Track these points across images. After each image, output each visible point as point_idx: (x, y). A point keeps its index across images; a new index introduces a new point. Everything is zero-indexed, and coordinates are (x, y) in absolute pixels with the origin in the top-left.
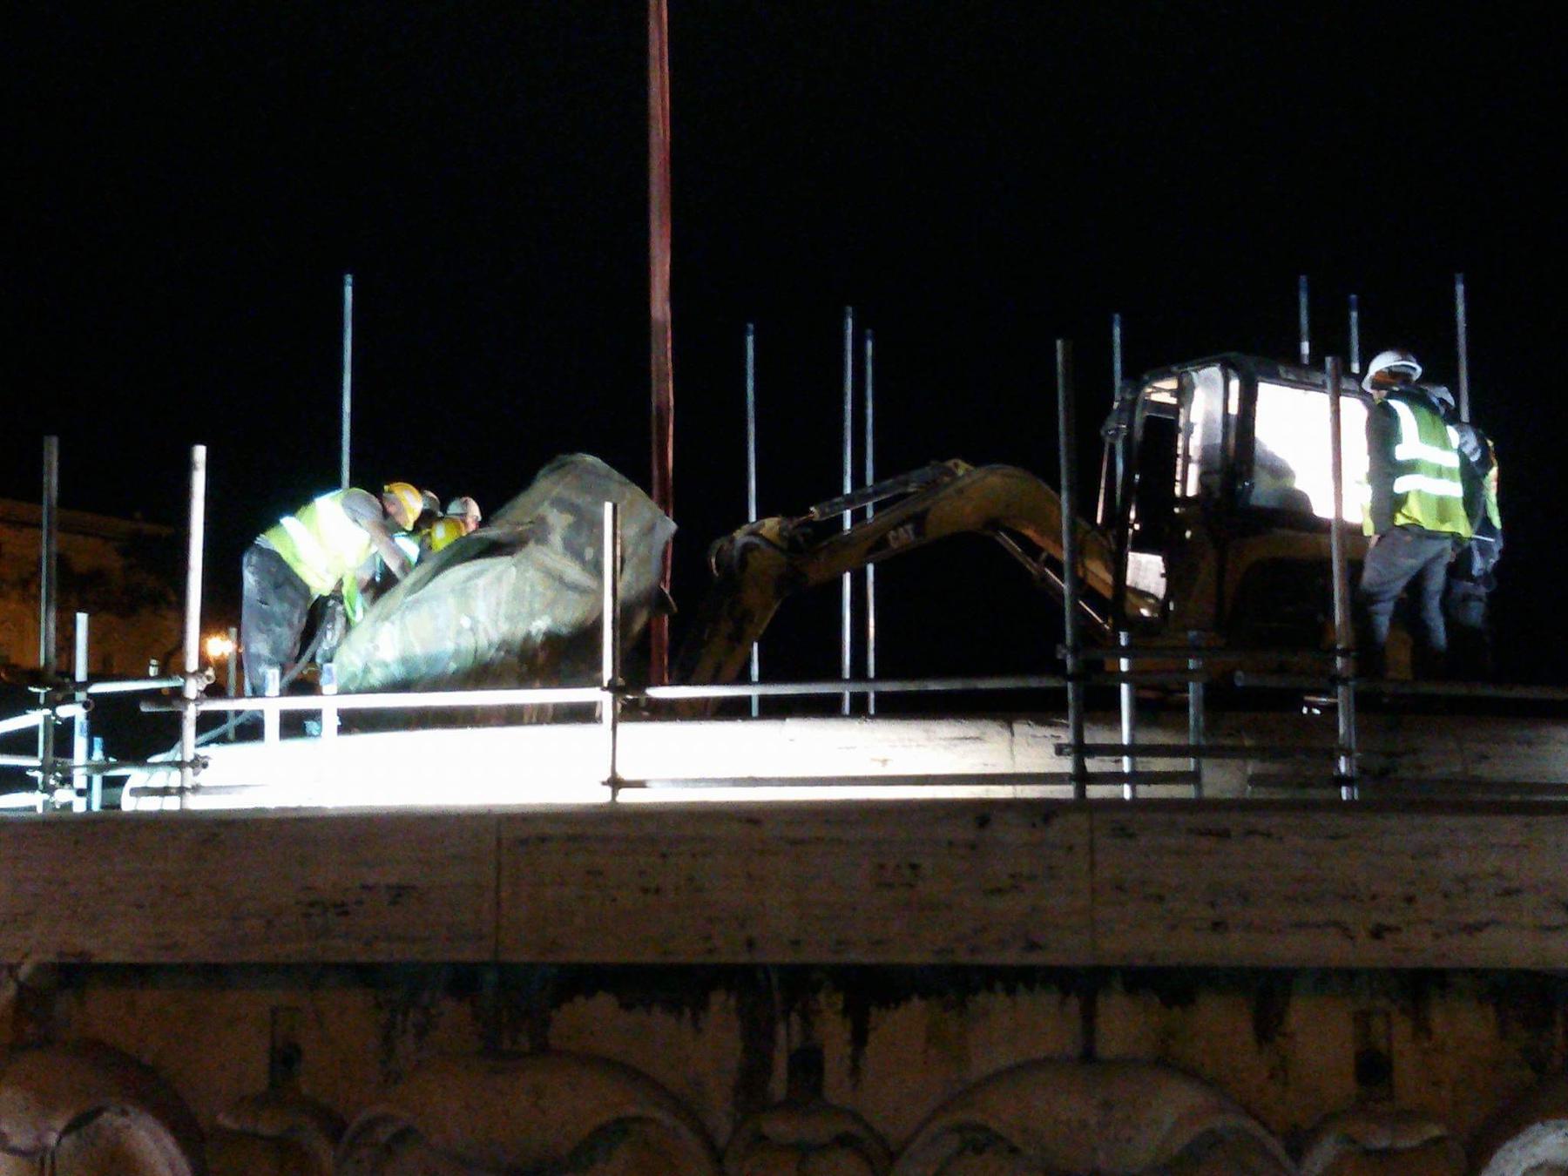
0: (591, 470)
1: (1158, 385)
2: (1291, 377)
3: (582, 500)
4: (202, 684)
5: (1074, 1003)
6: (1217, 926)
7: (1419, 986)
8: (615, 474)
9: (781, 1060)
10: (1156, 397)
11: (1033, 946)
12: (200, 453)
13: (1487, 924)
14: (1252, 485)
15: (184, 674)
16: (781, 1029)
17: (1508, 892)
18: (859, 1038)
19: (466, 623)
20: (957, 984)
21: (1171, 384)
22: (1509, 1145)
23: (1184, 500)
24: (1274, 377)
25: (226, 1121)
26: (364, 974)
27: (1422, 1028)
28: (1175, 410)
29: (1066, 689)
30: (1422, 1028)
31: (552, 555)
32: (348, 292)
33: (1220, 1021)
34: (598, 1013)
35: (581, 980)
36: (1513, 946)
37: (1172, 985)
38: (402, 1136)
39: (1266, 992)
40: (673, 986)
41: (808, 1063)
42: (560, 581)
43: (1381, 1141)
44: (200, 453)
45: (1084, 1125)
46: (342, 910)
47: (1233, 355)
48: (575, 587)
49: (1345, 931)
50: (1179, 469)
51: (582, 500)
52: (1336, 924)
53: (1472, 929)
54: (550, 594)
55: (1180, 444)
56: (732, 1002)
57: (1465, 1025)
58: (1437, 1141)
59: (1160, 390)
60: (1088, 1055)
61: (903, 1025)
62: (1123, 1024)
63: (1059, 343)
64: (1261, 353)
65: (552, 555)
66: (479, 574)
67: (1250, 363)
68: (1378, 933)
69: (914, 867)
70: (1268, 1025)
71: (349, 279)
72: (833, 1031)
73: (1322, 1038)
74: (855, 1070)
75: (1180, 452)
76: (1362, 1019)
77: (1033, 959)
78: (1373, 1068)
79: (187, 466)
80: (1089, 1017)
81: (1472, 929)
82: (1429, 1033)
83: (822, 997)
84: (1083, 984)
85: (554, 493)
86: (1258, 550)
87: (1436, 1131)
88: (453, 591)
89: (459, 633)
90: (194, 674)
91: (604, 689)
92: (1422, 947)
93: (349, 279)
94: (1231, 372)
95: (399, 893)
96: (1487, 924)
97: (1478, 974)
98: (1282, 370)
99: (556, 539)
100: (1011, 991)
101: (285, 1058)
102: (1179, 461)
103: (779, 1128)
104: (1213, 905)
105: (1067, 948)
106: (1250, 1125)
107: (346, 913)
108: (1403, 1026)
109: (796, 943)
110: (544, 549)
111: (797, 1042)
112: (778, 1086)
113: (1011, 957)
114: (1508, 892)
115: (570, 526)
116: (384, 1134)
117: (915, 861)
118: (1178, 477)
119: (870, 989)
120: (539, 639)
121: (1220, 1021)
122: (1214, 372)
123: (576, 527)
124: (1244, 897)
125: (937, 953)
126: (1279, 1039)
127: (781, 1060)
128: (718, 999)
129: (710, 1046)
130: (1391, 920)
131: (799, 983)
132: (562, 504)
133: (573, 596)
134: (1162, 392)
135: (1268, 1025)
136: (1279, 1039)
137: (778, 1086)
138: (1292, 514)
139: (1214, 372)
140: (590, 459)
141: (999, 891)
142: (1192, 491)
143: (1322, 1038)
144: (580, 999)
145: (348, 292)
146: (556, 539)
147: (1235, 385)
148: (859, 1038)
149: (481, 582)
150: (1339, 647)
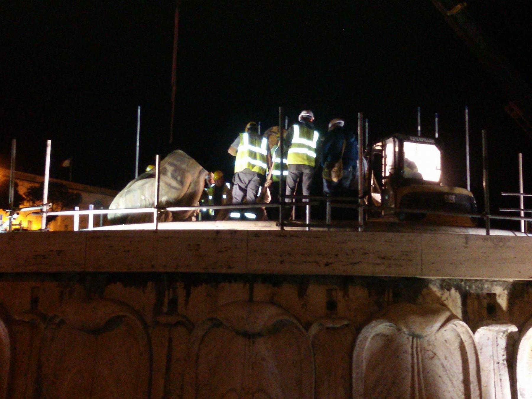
0: (181, 155)
1: (377, 144)
2: (414, 140)
3: (178, 163)
4: (48, 208)
5: (248, 285)
6: (282, 262)
7: (346, 281)
8: (187, 156)
9: (166, 301)
10: (377, 148)
11: (230, 267)
12: (49, 142)
13: (358, 263)
14: (403, 172)
15: (43, 205)
16: (167, 293)
17: (365, 254)
18: (188, 295)
19: (143, 198)
20: (215, 279)
21: (380, 144)
22: (366, 327)
23: (385, 177)
24: (409, 140)
25: (17, 318)
26: (56, 276)
27: (346, 294)
28: (381, 151)
29: (278, 208)
30: (346, 294)
31: (168, 179)
32: (139, 111)
33: (288, 292)
34: (117, 289)
35: (114, 278)
36: (366, 269)
37: (274, 280)
38: (62, 322)
39: (302, 283)
40: (135, 279)
41: (173, 303)
42: (170, 186)
43: (330, 325)
44: (49, 142)
45: (243, 318)
46: (44, 257)
47: (397, 134)
48: (175, 188)
49: (317, 263)
50: (383, 168)
51: (178, 163)
52: (315, 262)
53: (354, 264)
54: (167, 189)
55: (383, 161)
56: (154, 285)
57: (358, 294)
58: (347, 325)
59: (378, 146)
60: (251, 300)
61: (199, 292)
62: (261, 291)
63: (280, 108)
64: (405, 132)
65: (168, 179)
66: (146, 183)
67: (401, 137)
68: (327, 264)
69: (198, 245)
70: (302, 293)
71: (139, 107)
72: (181, 293)
73: (317, 295)
74: (186, 304)
75: (383, 163)
76: (329, 292)
77: (230, 271)
78: (332, 305)
79: (46, 146)
80: (252, 290)
81: (354, 264)
82: (348, 296)
83: (178, 283)
84: (250, 279)
85: (169, 161)
86: (406, 191)
87: (346, 323)
88: (139, 188)
89: (141, 200)
90: (45, 204)
91: (155, 208)
92: (340, 268)
93: (139, 107)
94: (396, 140)
95: (59, 252)
96: (358, 263)
97: (364, 278)
98: (411, 138)
99: (169, 174)
100: (230, 282)
101: (35, 301)
102: (383, 166)
103: (163, 319)
104: (281, 256)
105: (239, 269)
106: (295, 321)
107: (45, 258)
108: (340, 294)
109: (165, 266)
110: (166, 177)
111: (171, 297)
112: (165, 309)
113: (224, 271)
114: (365, 254)
115: (173, 170)
116: (57, 321)
117: (198, 243)
118: (383, 171)
119: (192, 280)
120: (164, 203)
121: (288, 292)
122: (391, 139)
123: (175, 171)
124: (290, 254)
125: (204, 269)
126: (305, 297)
127: (166, 301)
128: (150, 284)
129: (146, 297)
130: (330, 261)
131: (173, 278)
132: (171, 164)
133: (174, 191)
134: (378, 146)
135: (302, 293)
136: (305, 297)
137: (165, 309)
138: (417, 180)
139: (391, 139)
140: (180, 151)
141: (221, 251)
142: (388, 174)
143: (317, 295)
144: (109, 286)
145: (139, 111)
146: (169, 174)
147: (397, 143)
148: (188, 295)
149: (147, 186)
150: (360, 196)
